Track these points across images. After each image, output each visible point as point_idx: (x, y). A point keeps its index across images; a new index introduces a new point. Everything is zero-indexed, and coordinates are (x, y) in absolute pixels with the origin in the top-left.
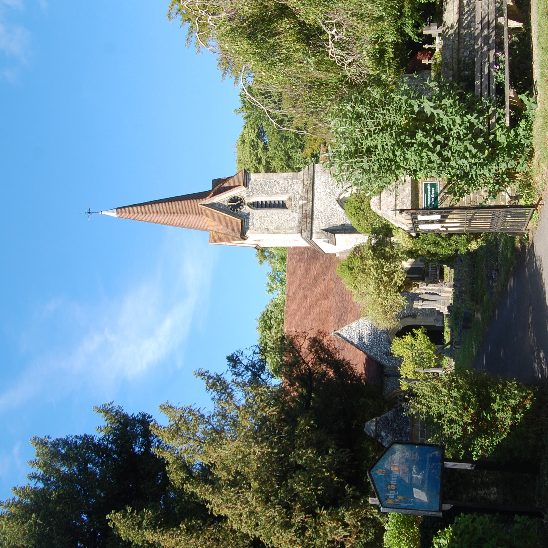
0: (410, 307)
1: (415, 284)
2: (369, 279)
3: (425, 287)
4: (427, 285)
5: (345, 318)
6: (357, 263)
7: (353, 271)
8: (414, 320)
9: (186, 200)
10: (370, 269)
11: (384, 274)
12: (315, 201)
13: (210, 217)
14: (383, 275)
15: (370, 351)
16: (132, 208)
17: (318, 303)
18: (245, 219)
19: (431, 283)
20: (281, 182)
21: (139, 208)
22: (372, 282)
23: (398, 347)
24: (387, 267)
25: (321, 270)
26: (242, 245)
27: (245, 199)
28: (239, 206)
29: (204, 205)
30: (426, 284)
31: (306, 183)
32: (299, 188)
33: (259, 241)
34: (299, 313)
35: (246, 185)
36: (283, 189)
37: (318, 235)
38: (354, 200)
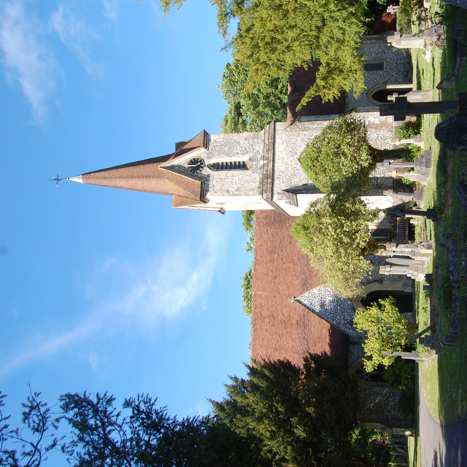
0: (376, 272)
1: (381, 245)
2: (326, 241)
3: (394, 249)
4: (397, 246)
5: (310, 282)
6: (313, 222)
7: (308, 231)
8: (380, 285)
10: (328, 228)
11: (344, 234)
12: (276, 161)
13: (171, 180)
14: (342, 235)
15: (333, 319)
17: (285, 266)
19: (402, 243)
20: (241, 142)
21: (103, 173)
22: (330, 244)
23: (364, 320)
24: (348, 225)
26: (206, 209)
28: (199, 167)
29: (164, 168)
30: (395, 244)
32: (260, 147)
33: (222, 204)
34: (266, 277)
35: (206, 145)
36: (243, 149)
38: (310, 150)
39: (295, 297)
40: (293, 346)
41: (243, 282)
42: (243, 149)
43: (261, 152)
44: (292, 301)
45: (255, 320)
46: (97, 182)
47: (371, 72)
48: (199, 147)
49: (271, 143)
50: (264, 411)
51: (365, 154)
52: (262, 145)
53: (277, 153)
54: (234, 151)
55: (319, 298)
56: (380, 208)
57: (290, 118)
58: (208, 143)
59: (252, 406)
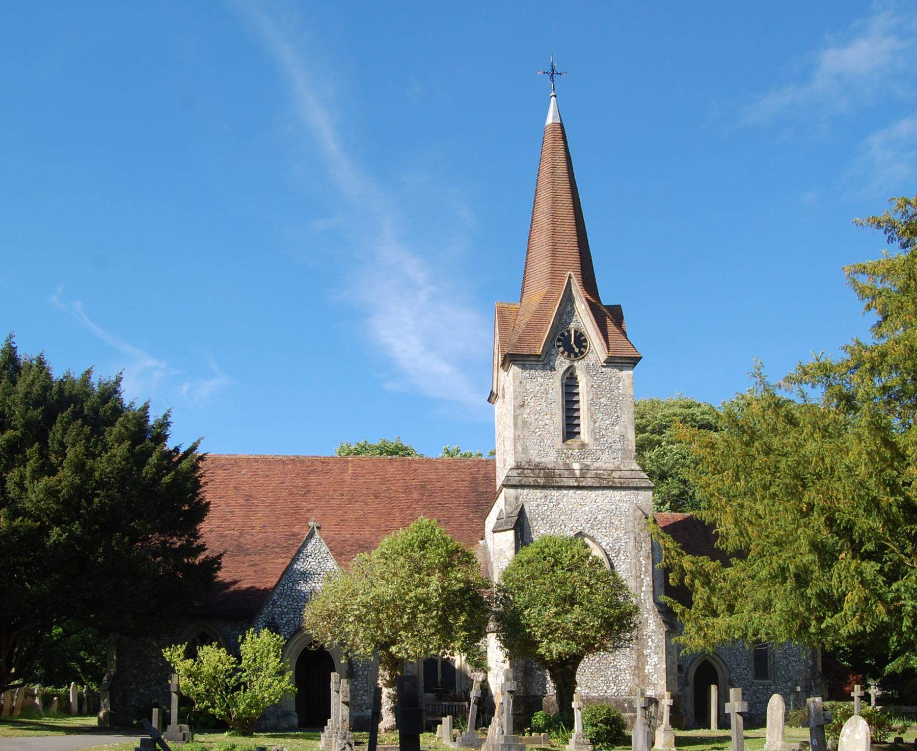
4: (346, 703)
6: (434, 557)
9: (571, 189)
12: (579, 492)
13: (547, 299)
16: (562, 151)
17: (396, 512)
18: (543, 362)
21: (562, 165)
23: (260, 644)
25: (457, 515)
27: (582, 361)
28: (569, 350)
29: (569, 284)
30: (348, 700)
31: (614, 475)
32: (605, 462)
33: (504, 397)
35: (613, 362)
36: (604, 432)
37: (512, 500)
38: (575, 551)
39: (318, 528)
40: (253, 528)
41: (392, 440)
42: (604, 432)
43: (596, 465)
44: (311, 524)
45: (302, 462)
46: (547, 154)
47: (752, 657)
48: (609, 349)
49: (613, 482)
50: (97, 474)
51: (561, 649)
52: (610, 466)
53: (593, 494)
54: (600, 416)
55: (319, 570)
56: (490, 675)
57: (673, 518)
58: (616, 367)
59: (106, 453)
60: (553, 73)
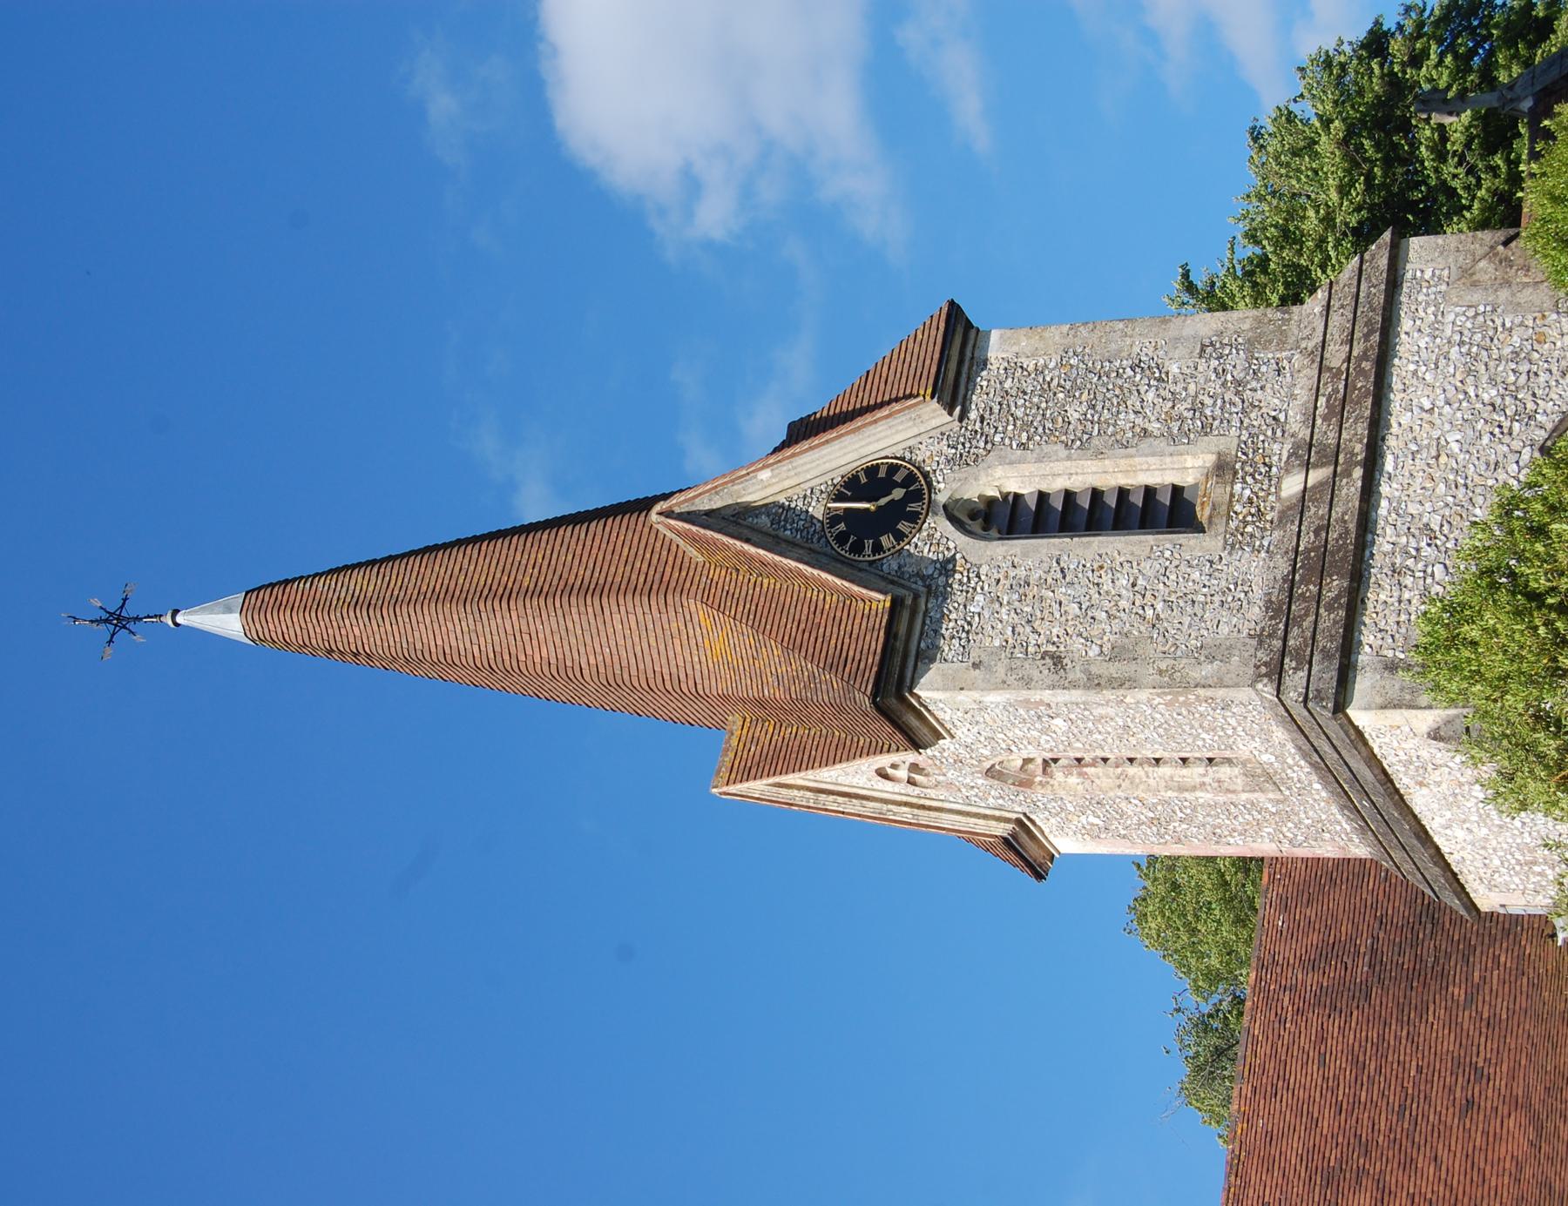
21: (357, 582)
25: (1450, 1045)
32: (1289, 396)
42: (1181, 407)
49: (1364, 356)
53: (1400, 418)
58: (971, 380)
60: (117, 620)
